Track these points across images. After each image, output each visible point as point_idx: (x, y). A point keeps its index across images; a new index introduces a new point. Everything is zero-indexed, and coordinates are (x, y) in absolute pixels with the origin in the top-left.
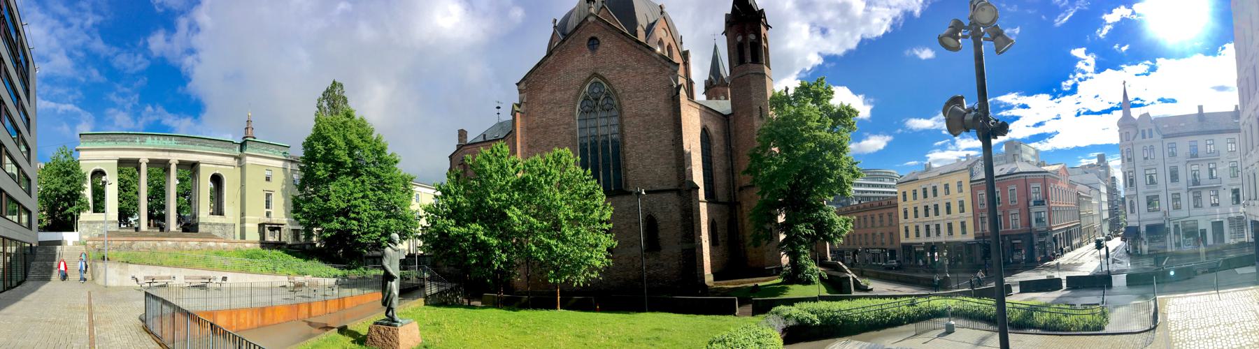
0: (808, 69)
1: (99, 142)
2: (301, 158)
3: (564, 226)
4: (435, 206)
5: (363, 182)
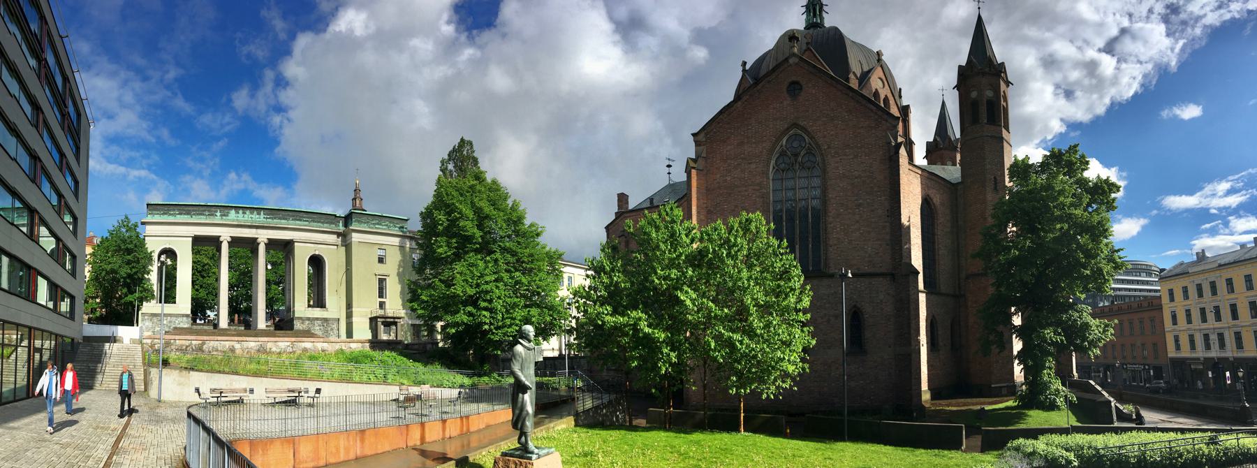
0: (1049, 137)
1: (171, 214)
2: (419, 231)
3: (752, 315)
4: (587, 289)
5: (496, 261)
